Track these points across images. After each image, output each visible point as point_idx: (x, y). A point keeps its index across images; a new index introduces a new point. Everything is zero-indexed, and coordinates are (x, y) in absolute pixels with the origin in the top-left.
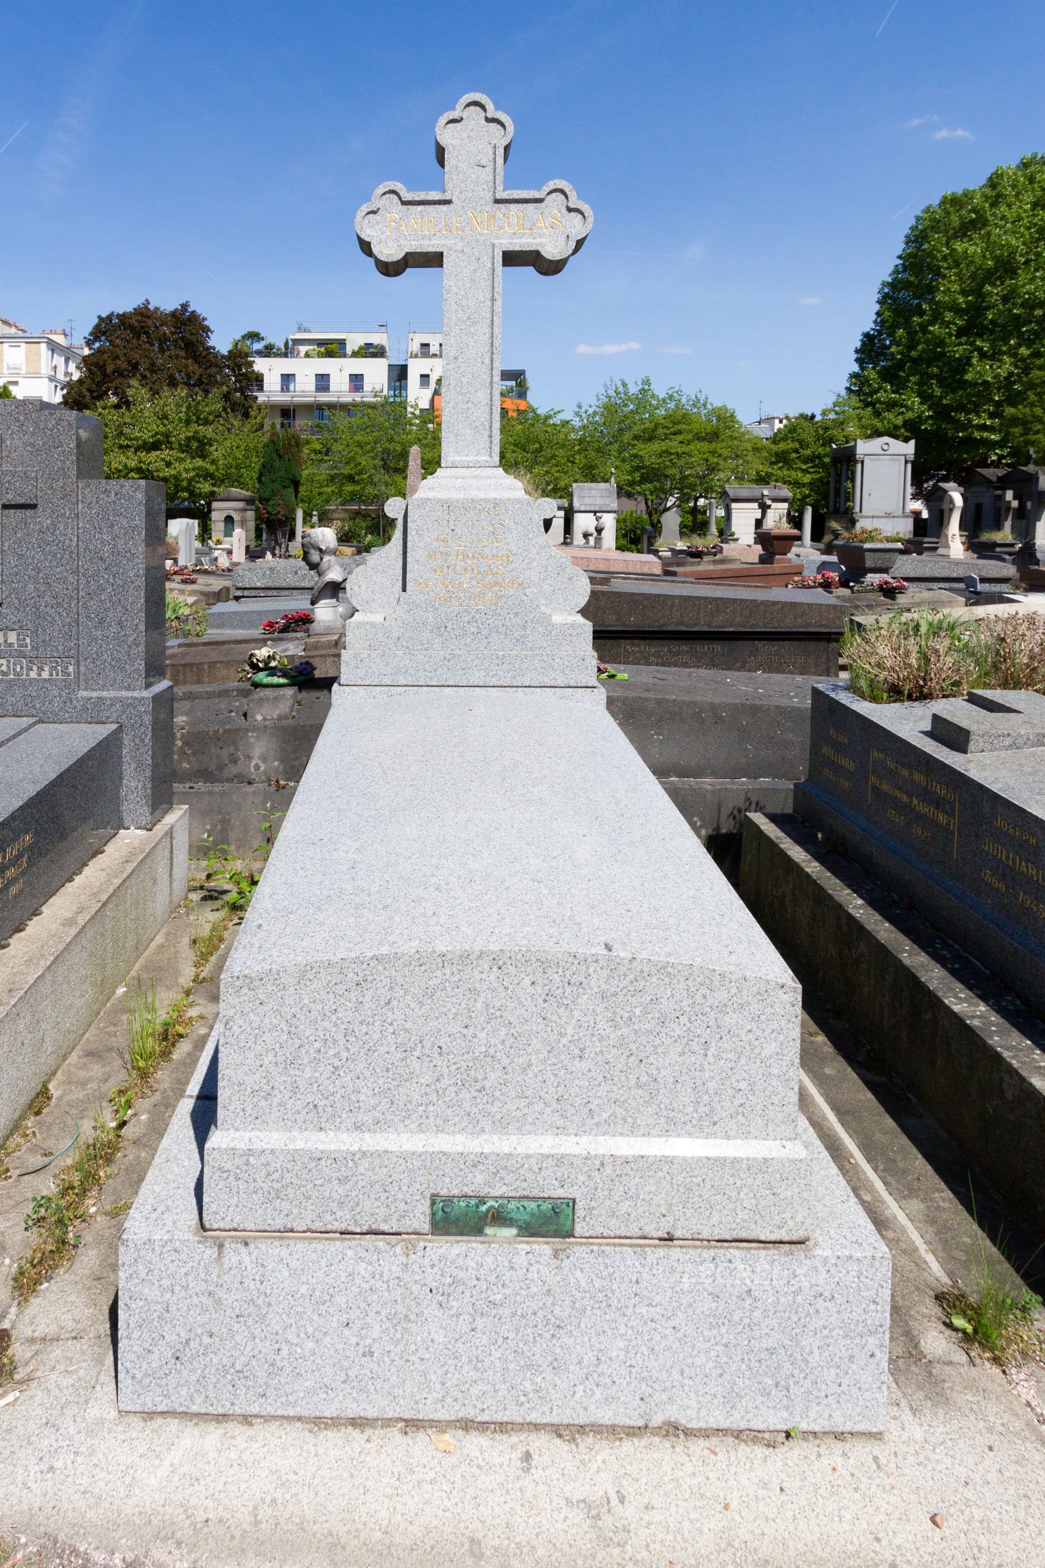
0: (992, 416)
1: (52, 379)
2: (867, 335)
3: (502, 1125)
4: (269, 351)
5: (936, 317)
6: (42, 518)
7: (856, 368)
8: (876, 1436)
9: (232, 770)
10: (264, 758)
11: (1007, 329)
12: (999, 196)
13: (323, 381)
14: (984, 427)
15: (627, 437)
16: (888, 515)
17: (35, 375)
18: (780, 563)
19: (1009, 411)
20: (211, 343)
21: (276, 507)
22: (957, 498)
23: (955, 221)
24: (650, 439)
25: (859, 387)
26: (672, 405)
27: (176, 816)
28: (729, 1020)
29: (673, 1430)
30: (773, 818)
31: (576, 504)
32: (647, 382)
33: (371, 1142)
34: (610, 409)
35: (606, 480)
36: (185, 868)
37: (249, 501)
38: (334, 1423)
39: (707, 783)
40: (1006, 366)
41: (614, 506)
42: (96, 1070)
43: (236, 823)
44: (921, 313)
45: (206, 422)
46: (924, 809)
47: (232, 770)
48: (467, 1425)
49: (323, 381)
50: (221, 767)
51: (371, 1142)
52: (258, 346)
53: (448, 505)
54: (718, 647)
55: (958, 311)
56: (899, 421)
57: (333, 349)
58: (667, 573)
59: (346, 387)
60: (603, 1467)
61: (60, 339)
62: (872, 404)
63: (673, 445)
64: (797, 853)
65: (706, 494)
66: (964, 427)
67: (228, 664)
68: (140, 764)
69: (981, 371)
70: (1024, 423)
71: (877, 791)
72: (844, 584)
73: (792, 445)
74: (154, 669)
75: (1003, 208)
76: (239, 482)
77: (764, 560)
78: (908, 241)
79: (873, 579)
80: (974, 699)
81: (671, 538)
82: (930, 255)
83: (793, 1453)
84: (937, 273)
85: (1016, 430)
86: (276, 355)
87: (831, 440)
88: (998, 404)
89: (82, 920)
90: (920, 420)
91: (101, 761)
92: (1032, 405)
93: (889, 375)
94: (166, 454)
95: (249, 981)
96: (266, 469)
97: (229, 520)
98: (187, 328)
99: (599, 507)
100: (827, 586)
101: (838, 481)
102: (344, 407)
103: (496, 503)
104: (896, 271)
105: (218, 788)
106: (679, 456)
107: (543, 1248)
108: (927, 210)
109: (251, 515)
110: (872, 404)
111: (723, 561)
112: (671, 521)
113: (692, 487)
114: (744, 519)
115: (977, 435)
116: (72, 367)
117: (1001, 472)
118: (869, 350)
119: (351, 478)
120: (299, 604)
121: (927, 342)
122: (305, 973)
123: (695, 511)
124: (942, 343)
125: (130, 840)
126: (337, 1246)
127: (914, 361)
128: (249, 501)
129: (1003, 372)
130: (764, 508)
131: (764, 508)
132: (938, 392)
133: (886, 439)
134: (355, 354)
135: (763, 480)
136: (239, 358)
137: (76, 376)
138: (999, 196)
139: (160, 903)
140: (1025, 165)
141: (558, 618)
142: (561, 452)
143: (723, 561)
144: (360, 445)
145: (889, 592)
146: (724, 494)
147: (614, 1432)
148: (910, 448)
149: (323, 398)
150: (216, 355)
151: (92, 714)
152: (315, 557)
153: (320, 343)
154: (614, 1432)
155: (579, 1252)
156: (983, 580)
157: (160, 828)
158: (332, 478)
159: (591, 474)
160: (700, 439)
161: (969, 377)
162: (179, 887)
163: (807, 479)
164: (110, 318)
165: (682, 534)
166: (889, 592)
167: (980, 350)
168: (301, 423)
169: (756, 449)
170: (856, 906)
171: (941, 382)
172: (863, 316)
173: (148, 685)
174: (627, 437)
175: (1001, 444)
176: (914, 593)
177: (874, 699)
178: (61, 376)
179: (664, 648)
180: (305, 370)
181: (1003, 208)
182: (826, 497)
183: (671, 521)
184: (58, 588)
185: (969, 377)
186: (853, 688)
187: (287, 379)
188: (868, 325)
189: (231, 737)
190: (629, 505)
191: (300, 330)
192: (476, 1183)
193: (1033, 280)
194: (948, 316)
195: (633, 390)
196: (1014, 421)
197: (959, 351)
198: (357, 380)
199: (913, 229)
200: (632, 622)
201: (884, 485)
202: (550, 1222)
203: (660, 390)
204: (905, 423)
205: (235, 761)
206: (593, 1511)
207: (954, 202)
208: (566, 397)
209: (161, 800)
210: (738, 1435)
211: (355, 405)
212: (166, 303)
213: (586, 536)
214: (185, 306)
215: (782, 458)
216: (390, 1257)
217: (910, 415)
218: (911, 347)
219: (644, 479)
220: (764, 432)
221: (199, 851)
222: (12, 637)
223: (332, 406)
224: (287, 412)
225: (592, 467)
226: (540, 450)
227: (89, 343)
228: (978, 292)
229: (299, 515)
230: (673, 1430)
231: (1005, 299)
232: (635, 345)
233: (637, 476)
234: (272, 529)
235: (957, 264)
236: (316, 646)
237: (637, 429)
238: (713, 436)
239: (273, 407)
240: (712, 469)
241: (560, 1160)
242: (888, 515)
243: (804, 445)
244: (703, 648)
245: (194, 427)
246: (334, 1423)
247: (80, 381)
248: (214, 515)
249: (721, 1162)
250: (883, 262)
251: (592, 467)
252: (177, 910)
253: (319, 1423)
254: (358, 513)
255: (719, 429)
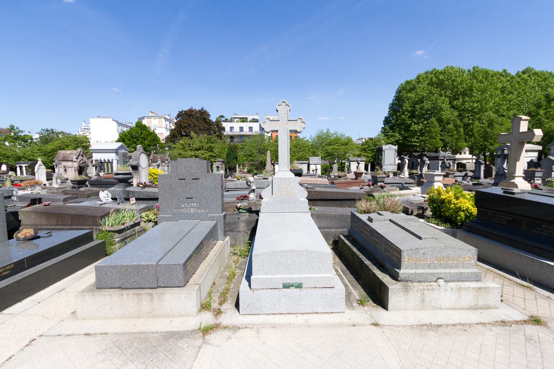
0: (418, 139)
1: (166, 128)
2: (386, 117)
3: (292, 274)
4: (226, 121)
5: (403, 113)
6: (200, 181)
7: (383, 126)
8: (344, 312)
9: (236, 230)
10: (243, 227)
11: (421, 116)
12: (419, 81)
13: (241, 129)
14: (415, 142)
15: (324, 145)
16: (391, 165)
17: (161, 127)
18: (359, 179)
19: (421, 138)
20: (210, 119)
21: (232, 165)
22: (407, 161)
23: (408, 88)
24: (330, 145)
25: (384, 131)
26: (335, 136)
27: (228, 238)
28: (323, 258)
29: (317, 313)
30: (344, 236)
31: (310, 162)
32: (328, 130)
33: (274, 276)
34: (319, 137)
35: (318, 156)
36: (229, 249)
37: (223, 162)
38: (270, 314)
39: (333, 230)
40: (421, 126)
41: (320, 163)
42: (222, 280)
43: (238, 240)
44: (400, 112)
45: (213, 143)
46: (366, 232)
47: (236, 230)
48: (288, 314)
49: (241, 129)
50: (234, 229)
51: (274, 276)
52: (223, 119)
53: (280, 179)
54: (338, 202)
55: (409, 112)
56: (394, 140)
57: (244, 120)
58: (333, 183)
59: (248, 130)
60: (306, 317)
61: (168, 117)
62: (387, 136)
63: (335, 147)
64: (347, 242)
65: (344, 159)
66: (410, 142)
67: (231, 207)
68: (221, 228)
69: (415, 127)
70: (424, 141)
71: (360, 230)
72: (373, 185)
73: (367, 146)
74: (223, 210)
75: (420, 85)
76: (220, 157)
77: (356, 179)
78: (397, 93)
79: (379, 184)
80: (378, 213)
81: (335, 172)
82: (402, 96)
83: (333, 314)
84: (404, 102)
85: (422, 143)
86: (229, 122)
87: (377, 145)
88: (419, 136)
89: (217, 255)
90: (399, 140)
91: (215, 227)
92: (426, 137)
93: (392, 128)
94: (202, 152)
95: (256, 255)
96: (228, 155)
97: (218, 167)
98: (203, 115)
99: (317, 164)
100: (369, 185)
101: (378, 156)
102: (248, 136)
103: (289, 178)
104: (393, 100)
105: (234, 233)
106: (337, 149)
107: (298, 289)
108: (401, 84)
109: (224, 166)
110: (387, 136)
111: (346, 179)
112: (335, 167)
113: (341, 158)
114: (354, 167)
115: (414, 144)
116: (171, 125)
117: (418, 154)
118: (387, 121)
119: (250, 155)
120: (246, 192)
121: (401, 120)
122: (264, 254)
123: (342, 163)
124: (404, 120)
125: (220, 243)
126: (270, 290)
127: (398, 125)
128: (223, 162)
129: (420, 128)
130: (358, 163)
131: (358, 163)
132: (403, 133)
133: (390, 145)
134: (250, 121)
135: (359, 156)
136: (218, 123)
137: (173, 127)
138: (419, 81)
139: (226, 255)
140: (426, 73)
141: (301, 200)
142: (307, 148)
143: (346, 179)
144: (252, 147)
145: (382, 187)
146: (349, 160)
147: (308, 313)
148: (396, 147)
149: (242, 133)
150: (212, 122)
151: (212, 219)
152: (249, 183)
153: (240, 118)
154: (308, 313)
155: (303, 290)
156: (406, 183)
157: (226, 240)
158: (245, 155)
159: (314, 154)
160: (343, 145)
161: (411, 129)
162: (229, 252)
163: (370, 155)
164: (182, 112)
165: (339, 170)
166: (382, 187)
167: (414, 122)
168: (236, 140)
169: (357, 148)
170: (355, 250)
171: (404, 130)
172: (385, 113)
173: (222, 212)
174: (324, 145)
175: (420, 146)
176: (388, 187)
177: (361, 213)
178: (168, 127)
179: (326, 203)
180: (237, 126)
181: (420, 85)
182: (375, 160)
183: (335, 167)
184: (204, 195)
185: (411, 129)
186: (358, 211)
187: (232, 128)
188: (386, 114)
189: (236, 223)
190: (325, 162)
191: (235, 115)
192: (289, 281)
193: (427, 104)
194: (406, 113)
195: (325, 132)
196: (422, 141)
197: (409, 122)
198: (251, 129)
199: (398, 89)
200: (319, 197)
201: (390, 156)
202: (299, 286)
203: (332, 132)
204: (395, 141)
205: (237, 228)
206: (305, 320)
207: (408, 82)
208: (308, 135)
209: (225, 235)
210: (325, 313)
211: (250, 135)
212: (197, 107)
213: (313, 171)
214: (202, 109)
215: (364, 150)
216: (277, 291)
217: (396, 139)
218: (397, 121)
219: (328, 156)
220: (360, 142)
221: (232, 246)
222: (195, 204)
223: (244, 136)
224: (232, 137)
225: (315, 152)
226: (300, 148)
227: (176, 119)
228: (414, 107)
229: (237, 166)
230: (317, 313)
231: (421, 109)
232: (327, 118)
233: (326, 155)
234: (230, 170)
235: (408, 100)
236: (251, 203)
237: (326, 142)
238: (346, 144)
239: (228, 136)
240: (346, 153)
241: (300, 278)
242: (391, 165)
243: (369, 146)
244: (335, 202)
245: (209, 144)
246: (270, 314)
247: (175, 129)
248: (214, 166)
249: (322, 277)
250: (390, 98)
251: (315, 152)
252: (229, 256)
253: (268, 314)
254: (252, 164)
255: (348, 142)
